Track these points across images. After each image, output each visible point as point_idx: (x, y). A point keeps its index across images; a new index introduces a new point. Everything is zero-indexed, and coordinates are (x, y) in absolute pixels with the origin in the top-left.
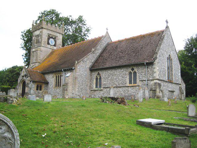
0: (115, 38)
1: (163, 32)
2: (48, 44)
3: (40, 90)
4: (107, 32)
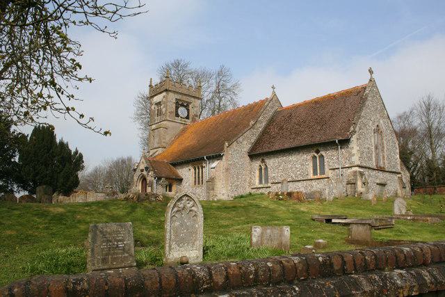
0: (286, 102)
1: (364, 88)
2: (177, 115)
4: (274, 92)
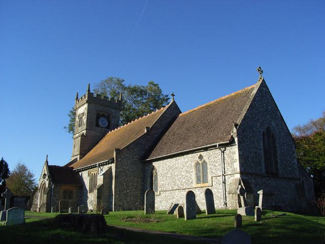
2: (98, 125)
3: (69, 198)
